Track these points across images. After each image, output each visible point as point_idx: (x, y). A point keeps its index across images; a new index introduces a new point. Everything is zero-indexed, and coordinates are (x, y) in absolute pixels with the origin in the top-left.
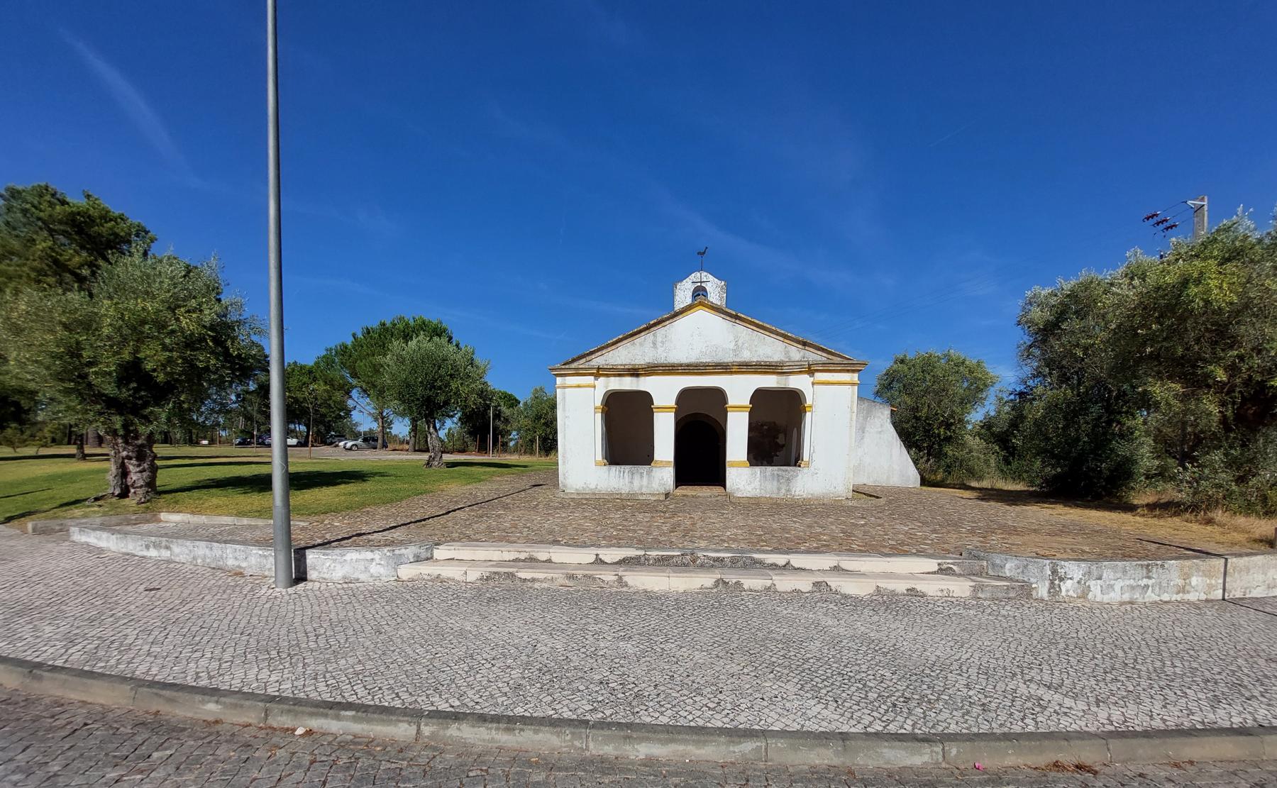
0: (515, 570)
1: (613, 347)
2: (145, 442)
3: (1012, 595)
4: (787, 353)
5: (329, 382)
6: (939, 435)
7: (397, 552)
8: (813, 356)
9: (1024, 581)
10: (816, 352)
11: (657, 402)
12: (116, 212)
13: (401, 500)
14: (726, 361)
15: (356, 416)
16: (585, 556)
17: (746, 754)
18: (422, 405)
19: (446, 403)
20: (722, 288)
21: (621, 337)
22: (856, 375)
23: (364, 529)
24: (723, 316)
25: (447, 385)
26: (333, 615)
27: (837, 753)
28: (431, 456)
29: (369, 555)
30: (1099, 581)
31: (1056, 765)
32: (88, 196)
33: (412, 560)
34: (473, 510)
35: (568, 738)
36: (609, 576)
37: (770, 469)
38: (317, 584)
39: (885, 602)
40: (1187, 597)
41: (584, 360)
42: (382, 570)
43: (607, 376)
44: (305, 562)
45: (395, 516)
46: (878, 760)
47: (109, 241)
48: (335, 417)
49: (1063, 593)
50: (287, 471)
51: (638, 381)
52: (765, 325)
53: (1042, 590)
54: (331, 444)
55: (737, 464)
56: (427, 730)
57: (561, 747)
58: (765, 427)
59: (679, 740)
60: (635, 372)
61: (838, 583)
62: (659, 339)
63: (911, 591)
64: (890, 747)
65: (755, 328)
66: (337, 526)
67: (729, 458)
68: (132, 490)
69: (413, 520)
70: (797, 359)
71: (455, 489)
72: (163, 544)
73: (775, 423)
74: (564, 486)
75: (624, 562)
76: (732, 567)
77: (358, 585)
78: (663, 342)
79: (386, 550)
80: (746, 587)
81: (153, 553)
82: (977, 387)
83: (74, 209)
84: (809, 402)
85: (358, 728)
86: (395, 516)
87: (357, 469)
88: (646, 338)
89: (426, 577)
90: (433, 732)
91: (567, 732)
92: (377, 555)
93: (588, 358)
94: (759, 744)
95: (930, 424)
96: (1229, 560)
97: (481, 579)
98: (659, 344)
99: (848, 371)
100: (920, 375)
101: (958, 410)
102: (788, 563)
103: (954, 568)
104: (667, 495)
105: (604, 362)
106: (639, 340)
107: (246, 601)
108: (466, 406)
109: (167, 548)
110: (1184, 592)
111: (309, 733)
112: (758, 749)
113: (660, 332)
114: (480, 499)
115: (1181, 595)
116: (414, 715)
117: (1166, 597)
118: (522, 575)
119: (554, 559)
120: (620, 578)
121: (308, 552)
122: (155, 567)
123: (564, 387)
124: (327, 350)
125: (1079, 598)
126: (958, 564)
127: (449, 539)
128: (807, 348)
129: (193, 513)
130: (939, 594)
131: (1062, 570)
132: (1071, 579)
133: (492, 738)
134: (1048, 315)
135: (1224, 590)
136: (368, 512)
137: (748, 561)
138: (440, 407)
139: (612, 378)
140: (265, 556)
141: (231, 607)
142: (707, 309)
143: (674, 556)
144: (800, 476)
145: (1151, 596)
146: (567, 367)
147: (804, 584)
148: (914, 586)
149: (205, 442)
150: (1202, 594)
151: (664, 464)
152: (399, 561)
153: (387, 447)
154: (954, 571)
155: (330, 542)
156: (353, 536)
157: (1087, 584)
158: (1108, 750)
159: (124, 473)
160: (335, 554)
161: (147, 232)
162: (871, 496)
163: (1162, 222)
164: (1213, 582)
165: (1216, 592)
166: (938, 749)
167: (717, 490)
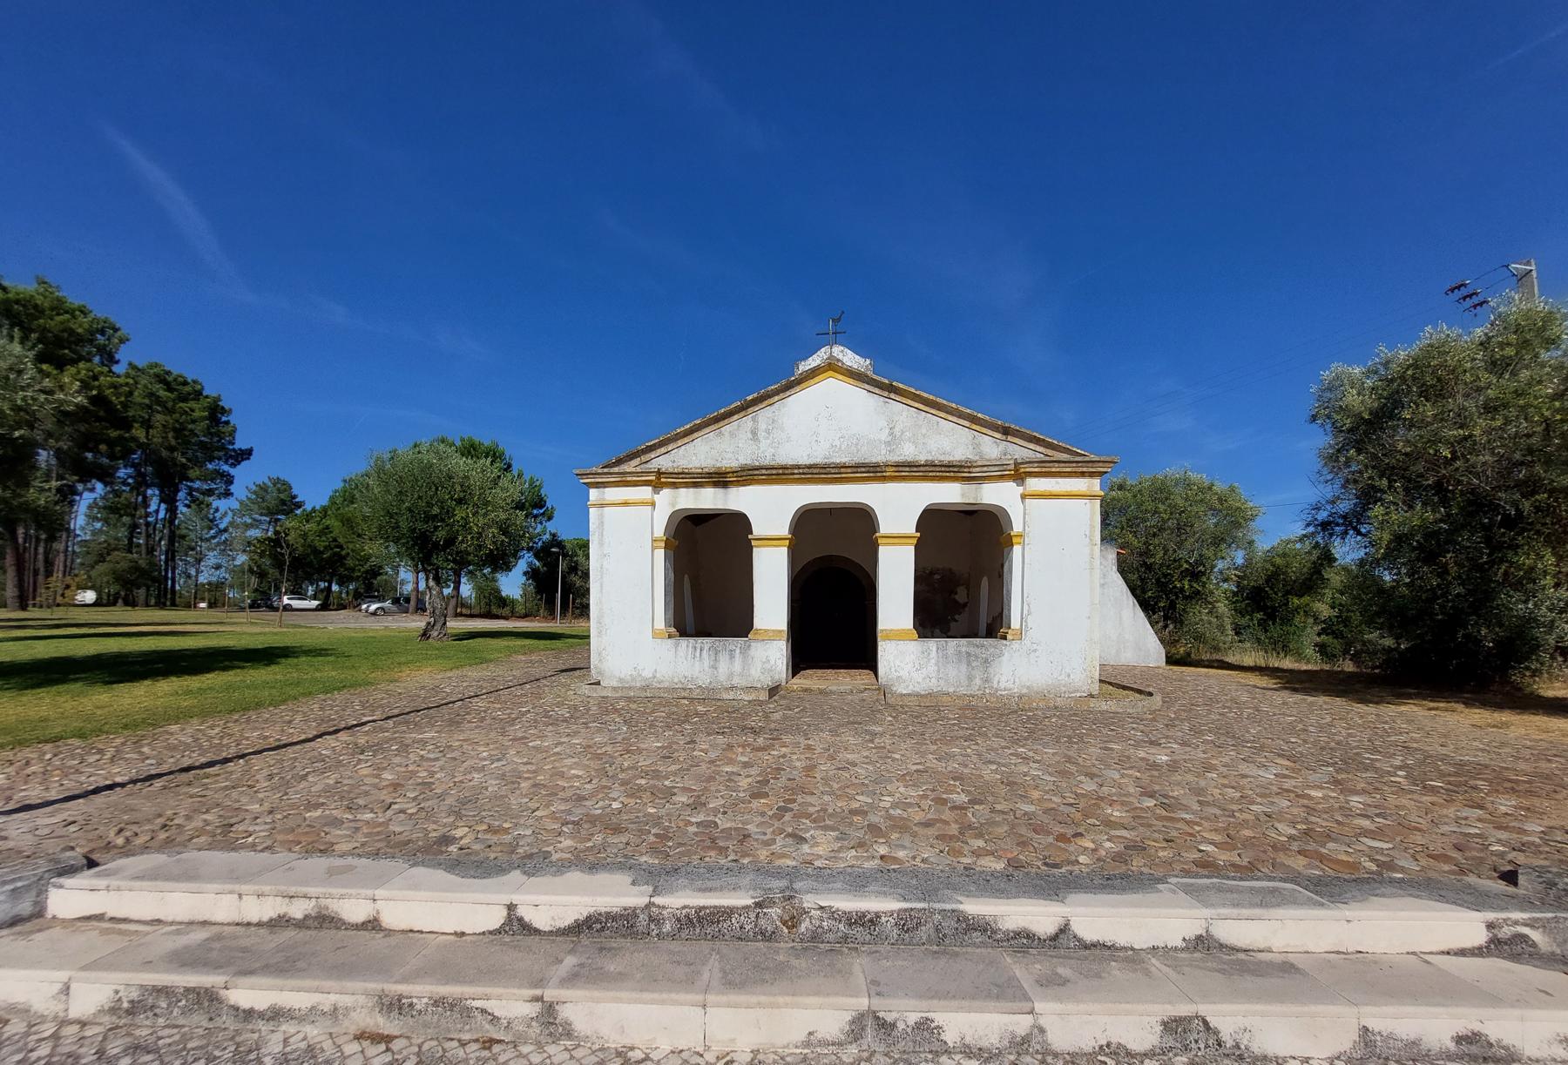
1: (686, 440)
6: (1182, 590)
8: (1020, 451)
12: (74, 300)
14: (874, 460)
22: (1096, 482)
24: (867, 387)
25: (450, 513)
28: (429, 623)
41: (636, 461)
43: (674, 486)
51: (726, 494)
52: (939, 400)
55: (898, 636)
58: (937, 577)
60: (720, 479)
61: (1241, 1022)
62: (762, 426)
65: (921, 407)
67: (881, 626)
73: (950, 570)
74: (599, 673)
76: (900, 941)
78: (768, 432)
80: (950, 1037)
82: (1233, 521)
83: (10, 295)
84: (1017, 527)
88: (740, 427)
95: (1165, 576)
97: (113, 1010)
98: (761, 434)
99: (1083, 474)
100: (1149, 506)
101: (1209, 553)
102: (1064, 929)
103: (1535, 935)
104: (773, 691)
105: (670, 464)
106: (728, 428)
108: (480, 546)
118: (248, 995)
120: (549, 1010)
123: (602, 506)
124: (345, 481)
128: (1009, 438)
134: (1372, 402)
139: (683, 491)
142: (841, 377)
146: (606, 470)
148: (1477, 1027)
149: (203, 605)
151: (770, 635)
154: (1534, 945)
162: (1125, 688)
163: (1470, 296)
167: (860, 678)
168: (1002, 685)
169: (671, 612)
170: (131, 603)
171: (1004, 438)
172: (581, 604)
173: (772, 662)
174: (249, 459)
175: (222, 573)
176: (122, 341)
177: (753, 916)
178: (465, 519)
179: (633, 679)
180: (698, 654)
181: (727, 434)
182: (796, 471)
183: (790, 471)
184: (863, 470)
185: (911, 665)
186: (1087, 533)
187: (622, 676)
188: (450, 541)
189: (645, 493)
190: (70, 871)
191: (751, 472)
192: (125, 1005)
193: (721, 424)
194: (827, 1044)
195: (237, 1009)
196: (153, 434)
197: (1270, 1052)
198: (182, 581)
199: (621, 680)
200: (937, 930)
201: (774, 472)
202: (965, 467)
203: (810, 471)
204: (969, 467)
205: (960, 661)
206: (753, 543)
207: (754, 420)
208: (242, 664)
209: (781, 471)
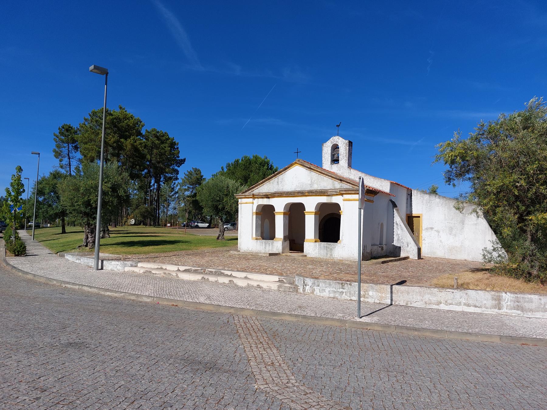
1: (262, 185)
3: (291, 290)
4: (334, 185)
7: (125, 263)
31: (173, 305)
32: (121, 108)
41: (250, 191)
43: (258, 198)
47: (126, 129)
49: (306, 291)
53: (301, 290)
55: (310, 241)
56: (80, 287)
60: (267, 196)
61: (236, 281)
62: (280, 180)
68: (89, 244)
76: (215, 275)
80: (210, 280)
85: (72, 286)
88: (274, 181)
89: (131, 271)
93: (252, 190)
97: (143, 273)
98: (280, 183)
103: (284, 280)
116: (79, 285)
119: (167, 269)
120: (177, 274)
123: (241, 204)
125: (311, 293)
128: (342, 182)
130: (267, 288)
132: (308, 285)
135: (392, 300)
137: (220, 273)
143: (199, 269)
144: (337, 247)
145: (344, 297)
146: (243, 194)
148: (259, 284)
150: (377, 300)
152: (125, 266)
154: (284, 281)
157: (314, 288)
159: (87, 238)
161: (141, 122)
164: (384, 295)
167: (301, 254)
168: (335, 257)
170: (145, 224)
171: (341, 182)
173: (279, 247)
174: (184, 163)
175: (176, 211)
176: (143, 126)
179: (247, 251)
181: (271, 183)
182: (284, 194)
184: (300, 193)
185: (312, 249)
187: (245, 250)
188: (223, 208)
189: (251, 200)
190: (140, 262)
191: (274, 195)
193: (270, 180)
194: (199, 280)
196: (152, 157)
198: (162, 214)
199: (244, 251)
201: (279, 194)
204: (327, 192)
206: (275, 214)
208: (166, 244)
209: (280, 194)
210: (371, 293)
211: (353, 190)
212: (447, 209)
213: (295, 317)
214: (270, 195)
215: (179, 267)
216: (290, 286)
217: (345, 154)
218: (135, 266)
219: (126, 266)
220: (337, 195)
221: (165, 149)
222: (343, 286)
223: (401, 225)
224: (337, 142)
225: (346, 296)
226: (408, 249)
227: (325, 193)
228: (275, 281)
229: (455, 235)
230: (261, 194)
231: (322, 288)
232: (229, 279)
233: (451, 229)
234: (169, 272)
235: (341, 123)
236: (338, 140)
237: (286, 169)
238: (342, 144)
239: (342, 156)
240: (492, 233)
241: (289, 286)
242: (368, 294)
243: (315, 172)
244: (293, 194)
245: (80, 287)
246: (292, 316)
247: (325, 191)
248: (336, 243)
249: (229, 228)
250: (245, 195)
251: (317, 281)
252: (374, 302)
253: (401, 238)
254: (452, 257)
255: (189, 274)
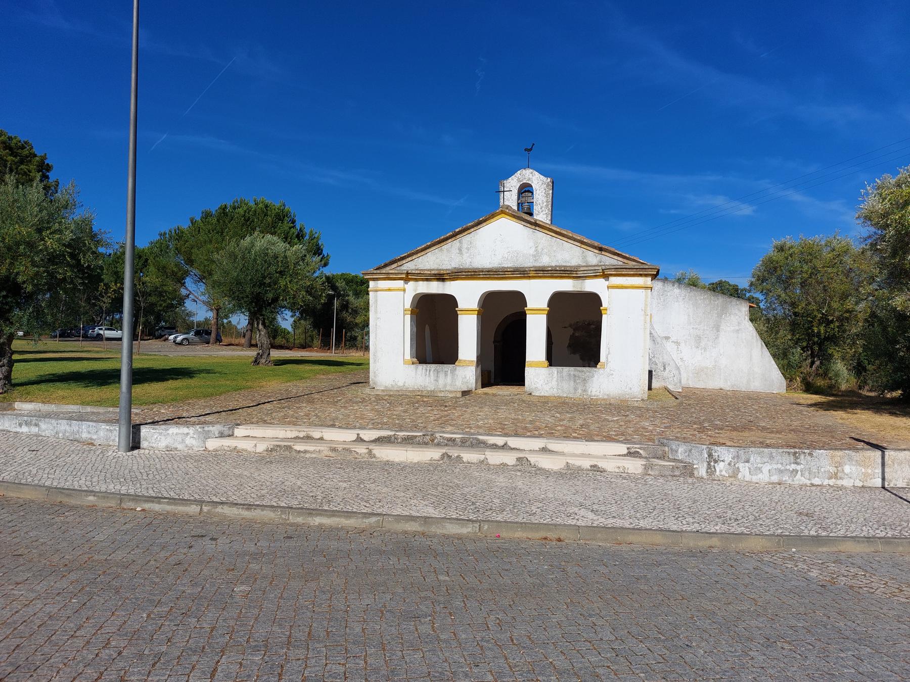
0: (292, 444)
1: (423, 253)
2: (6, 341)
3: (677, 473)
4: (584, 257)
5: (163, 270)
7: (206, 429)
8: (609, 260)
9: (690, 463)
10: (612, 256)
11: (461, 305)
13: (221, 394)
15: (189, 305)
16: (349, 436)
17: (372, 524)
18: (251, 303)
19: (275, 300)
20: (548, 186)
21: (429, 244)
23: (184, 415)
26: (158, 466)
27: (420, 525)
28: (258, 354)
29: (185, 430)
30: (747, 464)
33: (217, 436)
34: (279, 404)
35: (279, 513)
36: (362, 450)
37: (566, 369)
38: (147, 451)
39: (571, 473)
40: (840, 482)
42: (194, 442)
43: (416, 280)
44: (140, 435)
45: (211, 406)
46: (443, 530)
48: (167, 307)
49: (718, 473)
50: (131, 366)
51: (444, 285)
53: (702, 471)
54: (160, 337)
55: (537, 365)
57: (275, 518)
59: (337, 515)
60: (441, 277)
62: (465, 246)
63: (594, 467)
64: (450, 523)
65: (553, 234)
66: (163, 413)
69: (225, 410)
70: (594, 264)
71: (275, 385)
72: (34, 422)
74: (374, 383)
75: (379, 441)
77: (176, 452)
78: (468, 249)
79: (198, 427)
80: (465, 460)
81: (25, 429)
85: (169, 508)
86: (211, 406)
87: (185, 365)
88: (453, 245)
89: (226, 448)
90: (209, 510)
91: (279, 510)
92: (191, 430)
93: (399, 263)
94: (379, 518)
96: (886, 453)
98: (464, 251)
99: (641, 275)
102: (506, 444)
103: (641, 452)
104: (465, 393)
106: (446, 247)
107: (99, 458)
109: (36, 425)
110: (836, 478)
111: (143, 510)
112: (378, 521)
113: (466, 239)
114: (292, 395)
115: (833, 480)
117: (817, 481)
119: (325, 438)
120: (370, 451)
121: (142, 427)
122: (28, 439)
123: (376, 291)
124: (161, 235)
125: (731, 477)
126: (644, 449)
127: (248, 422)
128: (603, 253)
129: (43, 402)
130: (617, 470)
131: (716, 454)
132: (723, 461)
133: (240, 513)
135: (883, 479)
136: (189, 404)
137: (475, 441)
138: (269, 305)
140: (111, 431)
141: (90, 461)
144: (596, 376)
145: (799, 479)
146: (378, 272)
147: (509, 459)
148: (596, 463)
150: (858, 481)
151: (468, 363)
152: (207, 436)
153: (220, 341)
154: (641, 454)
155: (158, 422)
156: (175, 418)
157: (737, 466)
158: (579, 532)
160: (161, 428)
164: (870, 471)
165: (873, 480)
166: (477, 525)
168: (593, 394)
169: (414, 350)
171: (600, 252)
172: (351, 337)
173: (468, 378)
177: (422, 438)
178: (286, 286)
180: (428, 373)
182: (481, 273)
183: (477, 273)
184: (517, 273)
186: (643, 309)
189: (400, 283)
190: (238, 425)
191: (457, 274)
192: (270, 449)
193: (442, 244)
194: (435, 460)
195: (296, 450)
197: (543, 467)
200: (471, 443)
201: (469, 274)
202: (574, 271)
203: (489, 273)
204: (576, 271)
205: (570, 379)
206: (458, 312)
207: (460, 242)
209: (473, 273)
210: (847, 469)
211: (632, 269)
212: (691, 306)
213: (867, 544)
214: (447, 274)
215: (360, 432)
216: (673, 464)
217: (545, 204)
218: (229, 436)
219: (209, 438)
220: (596, 276)
221: (29, 175)
222: (797, 458)
223: (652, 334)
224: (529, 179)
225: (803, 478)
226: (666, 374)
227: (572, 273)
228: (619, 454)
229: (705, 349)
230: (426, 272)
231: (756, 466)
232: (516, 455)
233: (698, 339)
234: (345, 446)
235: (533, 144)
236: (531, 176)
237: (479, 223)
238: (540, 184)
239: (540, 207)
240: (761, 344)
241: (672, 465)
242: (843, 471)
243: (544, 231)
244: (501, 273)
245: (205, 509)
246: (858, 541)
247: (572, 269)
248: (594, 369)
249: (190, 341)
250: (388, 273)
251: (745, 452)
252: (854, 486)
253: (653, 356)
254: (700, 385)
255: (405, 449)
